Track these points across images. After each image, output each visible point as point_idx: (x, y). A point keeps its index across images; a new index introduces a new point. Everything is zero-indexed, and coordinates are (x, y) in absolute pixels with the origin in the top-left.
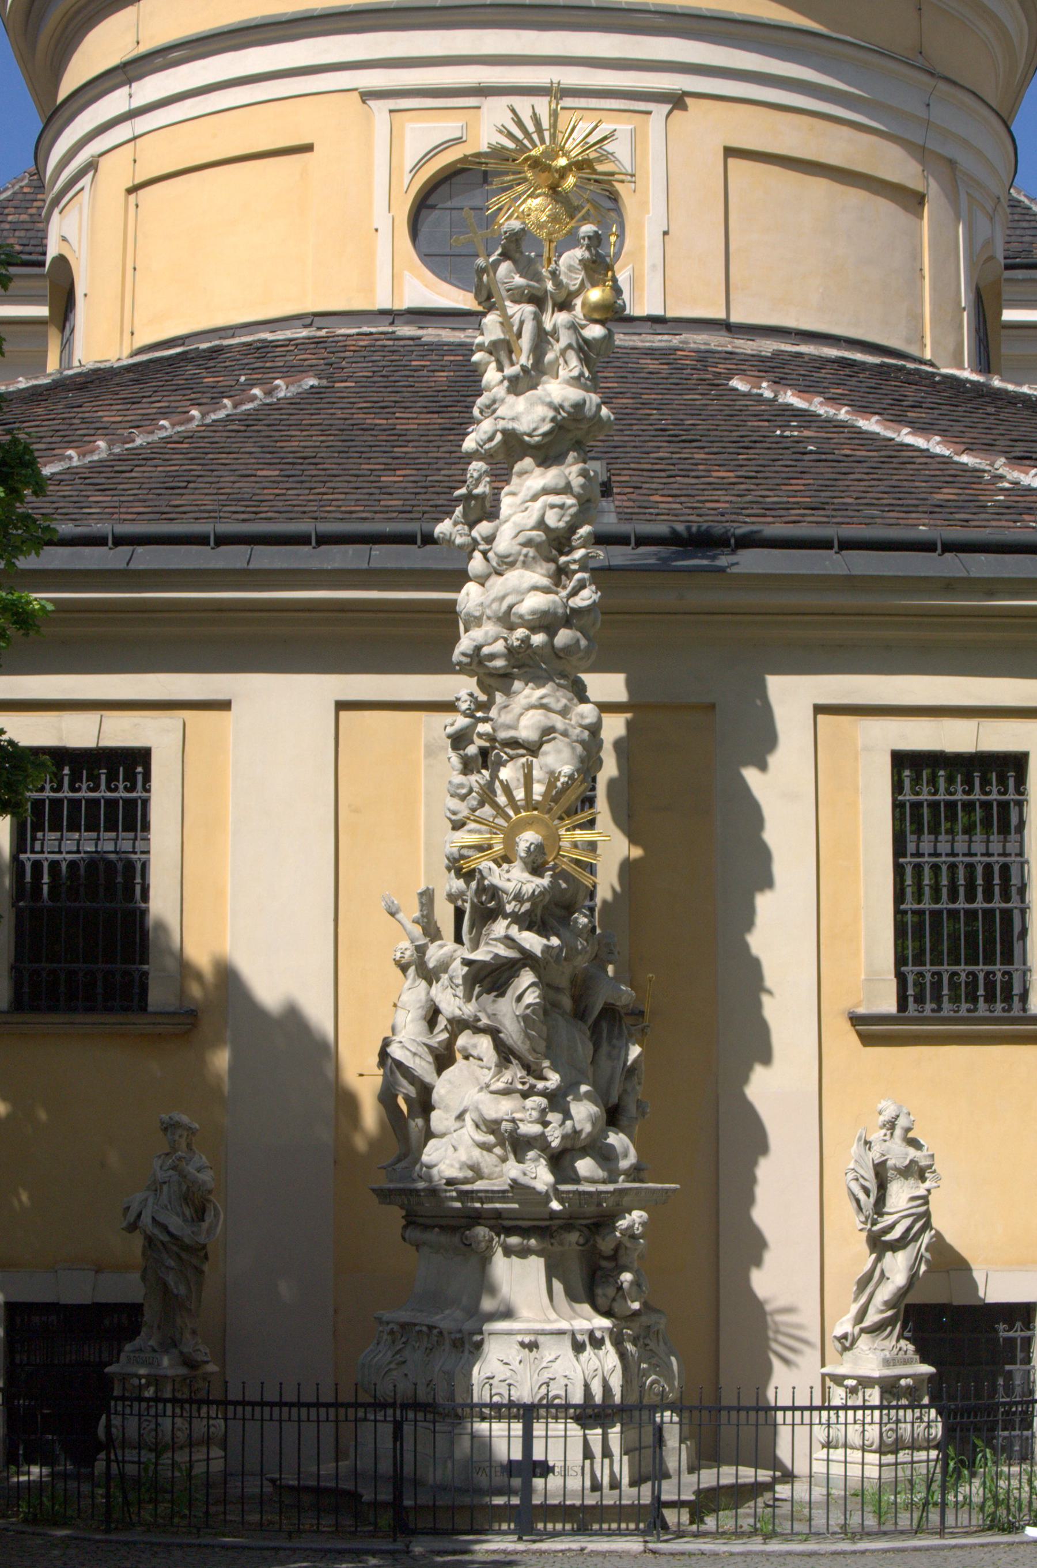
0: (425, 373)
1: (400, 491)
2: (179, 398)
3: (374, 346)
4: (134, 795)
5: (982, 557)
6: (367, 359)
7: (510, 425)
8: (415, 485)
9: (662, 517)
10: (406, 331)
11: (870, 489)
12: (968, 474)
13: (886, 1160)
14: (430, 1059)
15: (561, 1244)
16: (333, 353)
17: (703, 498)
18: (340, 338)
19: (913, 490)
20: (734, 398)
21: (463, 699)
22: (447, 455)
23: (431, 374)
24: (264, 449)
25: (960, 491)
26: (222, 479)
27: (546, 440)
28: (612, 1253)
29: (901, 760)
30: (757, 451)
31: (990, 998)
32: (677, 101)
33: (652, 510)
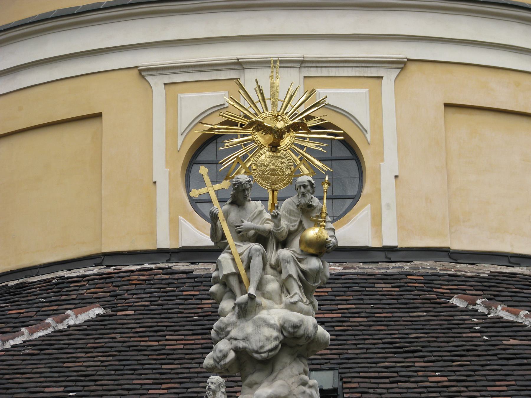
3: (152, 279)
6: (147, 291)
7: (241, 344)
10: (181, 266)
18: (125, 274)
23: (199, 302)
32: (402, 64)
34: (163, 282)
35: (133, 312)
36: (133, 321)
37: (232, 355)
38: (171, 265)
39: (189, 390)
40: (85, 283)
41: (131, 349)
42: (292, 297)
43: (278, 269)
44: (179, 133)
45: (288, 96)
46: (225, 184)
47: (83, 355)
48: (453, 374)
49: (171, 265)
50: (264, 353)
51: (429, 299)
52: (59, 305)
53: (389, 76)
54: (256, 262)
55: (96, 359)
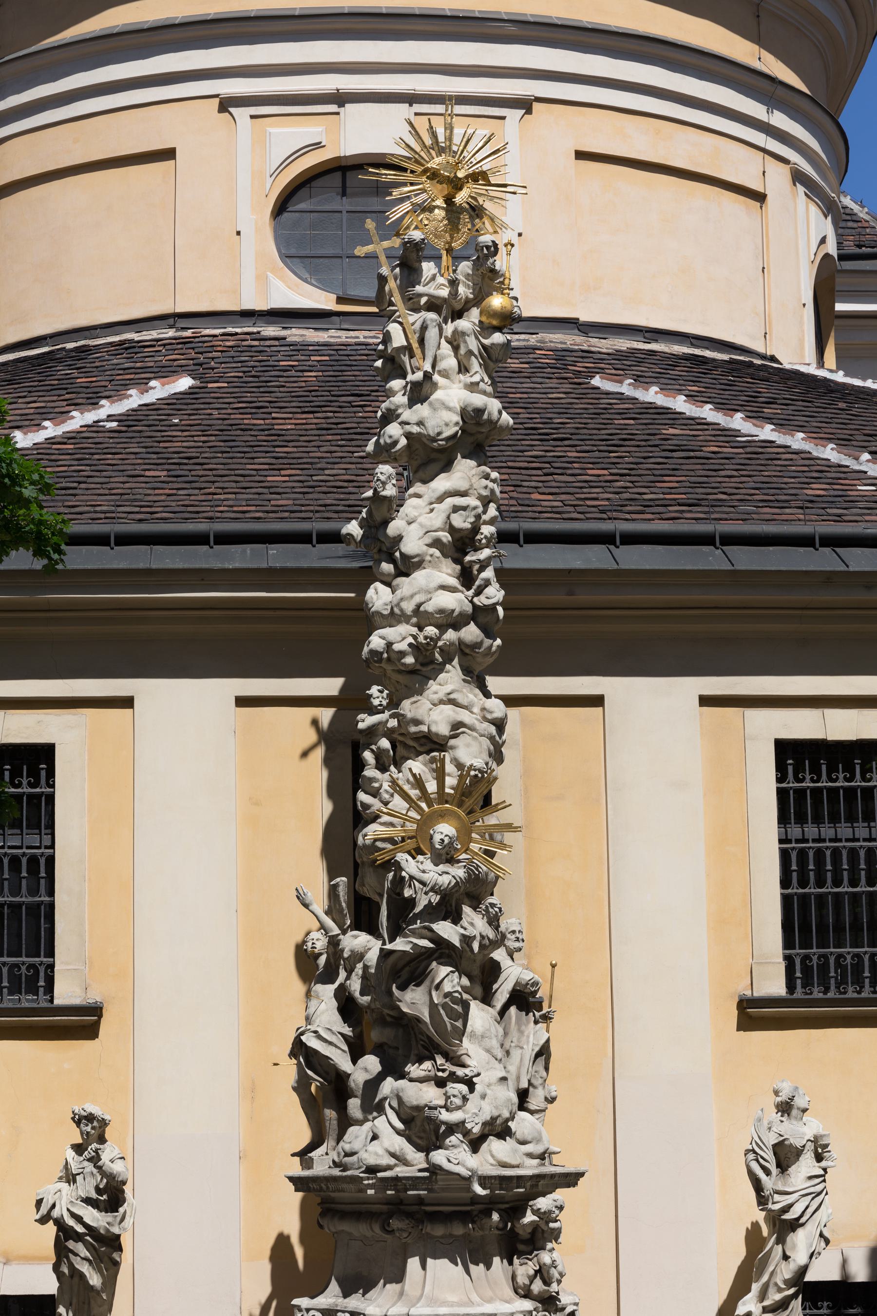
0: (293, 373)
1: (288, 490)
2: (55, 398)
3: (239, 347)
4: (38, 790)
5: (858, 551)
6: (236, 359)
7: (415, 429)
8: (300, 484)
9: (546, 515)
10: (271, 331)
11: (741, 485)
12: (834, 469)
13: (785, 1140)
14: (346, 1048)
15: (482, 1228)
16: (201, 353)
17: (583, 496)
18: (206, 339)
19: (783, 486)
20: (598, 396)
21: (374, 696)
22: (328, 455)
23: (300, 374)
24: (149, 450)
25: (827, 487)
26: (112, 480)
27: (450, 444)
28: (528, 1236)
29: (785, 750)
30: (627, 449)
31: (841, 983)
32: (525, 105)
33: (534, 509)
34: (253, 349)
35: (226, 385)
36: (229, 395)
37: (403, 442)
38: (259, 329)
39: (315, 478)
40: (161, 348)
41: (234, 427)
42: (471, 376)
43: (455, 343)
44: (268, 175)
45: (465, 140)
46: (396, 242)
47: (179, 433)
48: (613, 466)
49: (259, 329)
50: (441, 440)
51: (566, 378)
52: (136, 374)
53: (514, 115)
54: (432, 335)
55: (196, 439)
